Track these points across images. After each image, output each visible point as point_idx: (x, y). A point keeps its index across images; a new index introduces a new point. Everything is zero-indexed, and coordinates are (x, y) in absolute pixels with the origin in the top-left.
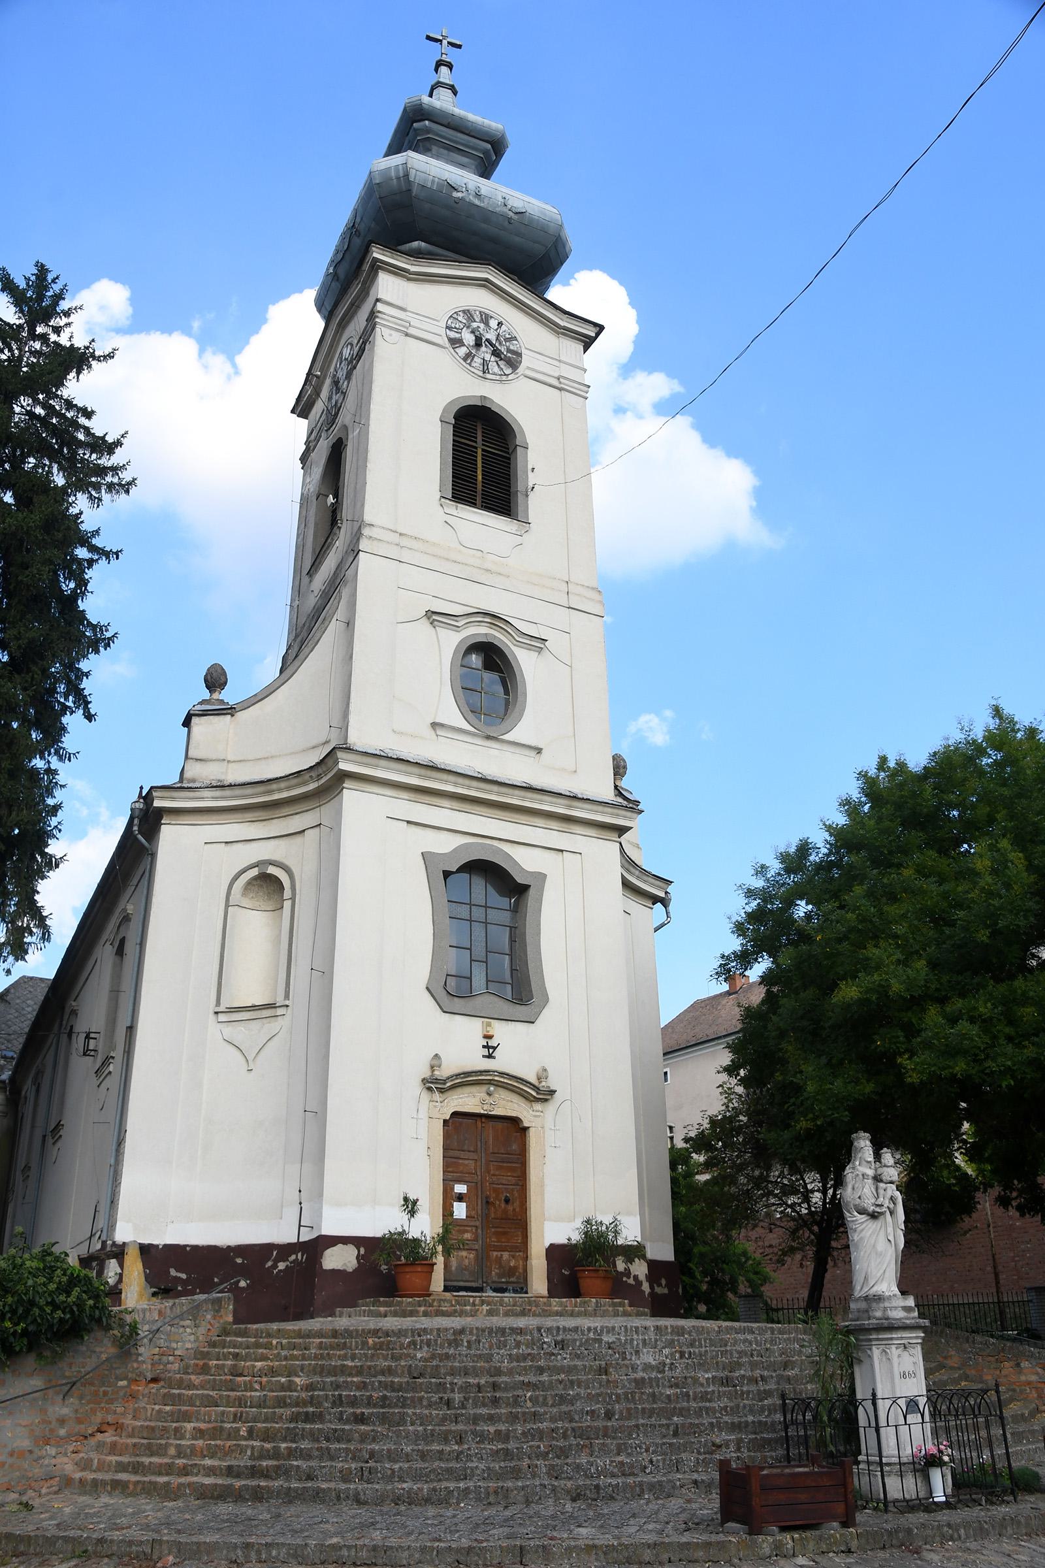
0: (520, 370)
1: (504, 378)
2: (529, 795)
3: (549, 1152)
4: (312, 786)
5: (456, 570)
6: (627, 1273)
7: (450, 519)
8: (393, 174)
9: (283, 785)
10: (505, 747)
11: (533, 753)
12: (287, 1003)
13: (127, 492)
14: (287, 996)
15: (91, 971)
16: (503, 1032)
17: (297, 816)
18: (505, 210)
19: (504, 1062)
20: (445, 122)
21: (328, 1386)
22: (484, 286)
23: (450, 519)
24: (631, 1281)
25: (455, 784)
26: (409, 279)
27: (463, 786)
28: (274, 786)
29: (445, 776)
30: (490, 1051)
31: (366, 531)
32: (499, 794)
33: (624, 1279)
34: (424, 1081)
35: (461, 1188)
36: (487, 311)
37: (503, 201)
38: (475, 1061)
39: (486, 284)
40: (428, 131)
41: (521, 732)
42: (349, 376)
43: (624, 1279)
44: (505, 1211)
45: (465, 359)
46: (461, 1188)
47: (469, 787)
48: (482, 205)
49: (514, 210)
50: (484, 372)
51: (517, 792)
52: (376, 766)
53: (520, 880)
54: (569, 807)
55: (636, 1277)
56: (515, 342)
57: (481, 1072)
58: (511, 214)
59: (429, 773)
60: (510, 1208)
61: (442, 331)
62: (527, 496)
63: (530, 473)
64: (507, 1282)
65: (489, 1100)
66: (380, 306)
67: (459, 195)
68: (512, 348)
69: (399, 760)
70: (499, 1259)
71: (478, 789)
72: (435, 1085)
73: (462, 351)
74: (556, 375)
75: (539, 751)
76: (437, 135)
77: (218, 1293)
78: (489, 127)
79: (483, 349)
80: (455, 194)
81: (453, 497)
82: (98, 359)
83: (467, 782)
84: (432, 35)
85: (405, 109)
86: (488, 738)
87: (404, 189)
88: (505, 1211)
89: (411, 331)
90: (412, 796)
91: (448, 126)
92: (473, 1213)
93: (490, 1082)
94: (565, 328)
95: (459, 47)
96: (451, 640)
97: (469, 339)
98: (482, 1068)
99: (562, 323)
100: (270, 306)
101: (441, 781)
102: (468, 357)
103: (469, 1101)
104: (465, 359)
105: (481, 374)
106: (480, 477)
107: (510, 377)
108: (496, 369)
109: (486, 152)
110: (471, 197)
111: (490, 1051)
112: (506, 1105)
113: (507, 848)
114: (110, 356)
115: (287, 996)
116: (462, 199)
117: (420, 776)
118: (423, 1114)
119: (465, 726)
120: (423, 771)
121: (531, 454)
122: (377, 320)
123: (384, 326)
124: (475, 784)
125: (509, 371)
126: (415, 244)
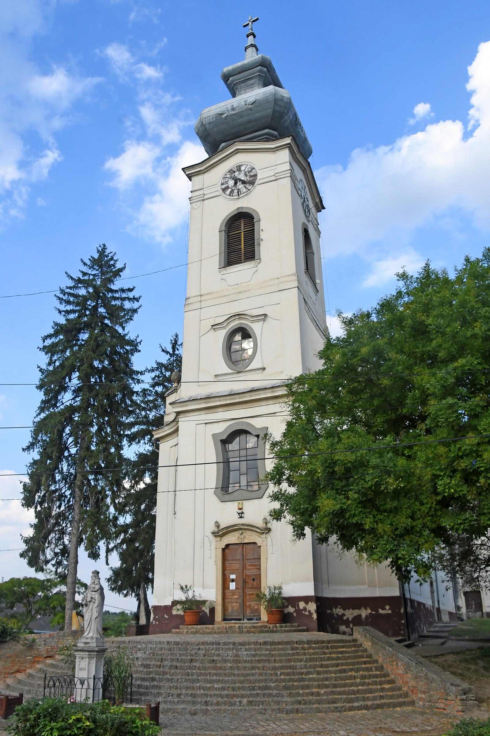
2: (253, 393)
3: (270, 556)
5: (225, 300)
6: (305, 609)
7: (223, 277)
11: (261, 371)
13: (132, 320)
18: (247, 106)
20: (237, 73)
22: (238, 152)
23: (223, 277)
24: (307, 613)
25: (220, 401)
26: (204, 173)
27: (223, 400)
29: (214, 399)
30: (241, 515)
32: (240, 398)
33: (303, 612)
34: (213, 533)
35: (233, 577)
38: (235, 520)
39: (237, 151)
40: (233, 81)
43: (303, 612)
44: (253, 585)
46: (233, 577)
47: (226, 400)
48: (236, 112)
51: (247, 394)
52: (187, 405)
54: (273, 392)
55: (309, 611)
58: (250, 106)
59: (207, 400)
60: (255, 583)
63: (261, 233)
64: (254, 616)
67: (225, 115)
68: (252, 174)
69: (193, 400)
70: (250, 606)
71: (230, 399)
73: (228, 192)
74: (273, 174)
75: (264, 369)
78: (255, 60)
79: (238, 184)
80: (223, 116)
83: (224, 398)
84: (245, 24)
86: (239, 372)
89: (206, 197)
90: (206, 411)
91: (239, 73)
92: (238, 587)
93: (241, 529)
95: (257, 19)
97: (231, 183)
99: (273, 146)
100: (469, 68)
101: (214, 401)
102: (232, 191)
103: (232, 538)
105: (237, 197)
108: (245, 190)
109: (260, 71)
111: (241, 515)
112: (250, 537)
113: (249, 421)
116: (227, 116)
117: (205, 403)
118: (213, 547)
120: (205, 401)
124: (228, 398)
126: (221, 147)
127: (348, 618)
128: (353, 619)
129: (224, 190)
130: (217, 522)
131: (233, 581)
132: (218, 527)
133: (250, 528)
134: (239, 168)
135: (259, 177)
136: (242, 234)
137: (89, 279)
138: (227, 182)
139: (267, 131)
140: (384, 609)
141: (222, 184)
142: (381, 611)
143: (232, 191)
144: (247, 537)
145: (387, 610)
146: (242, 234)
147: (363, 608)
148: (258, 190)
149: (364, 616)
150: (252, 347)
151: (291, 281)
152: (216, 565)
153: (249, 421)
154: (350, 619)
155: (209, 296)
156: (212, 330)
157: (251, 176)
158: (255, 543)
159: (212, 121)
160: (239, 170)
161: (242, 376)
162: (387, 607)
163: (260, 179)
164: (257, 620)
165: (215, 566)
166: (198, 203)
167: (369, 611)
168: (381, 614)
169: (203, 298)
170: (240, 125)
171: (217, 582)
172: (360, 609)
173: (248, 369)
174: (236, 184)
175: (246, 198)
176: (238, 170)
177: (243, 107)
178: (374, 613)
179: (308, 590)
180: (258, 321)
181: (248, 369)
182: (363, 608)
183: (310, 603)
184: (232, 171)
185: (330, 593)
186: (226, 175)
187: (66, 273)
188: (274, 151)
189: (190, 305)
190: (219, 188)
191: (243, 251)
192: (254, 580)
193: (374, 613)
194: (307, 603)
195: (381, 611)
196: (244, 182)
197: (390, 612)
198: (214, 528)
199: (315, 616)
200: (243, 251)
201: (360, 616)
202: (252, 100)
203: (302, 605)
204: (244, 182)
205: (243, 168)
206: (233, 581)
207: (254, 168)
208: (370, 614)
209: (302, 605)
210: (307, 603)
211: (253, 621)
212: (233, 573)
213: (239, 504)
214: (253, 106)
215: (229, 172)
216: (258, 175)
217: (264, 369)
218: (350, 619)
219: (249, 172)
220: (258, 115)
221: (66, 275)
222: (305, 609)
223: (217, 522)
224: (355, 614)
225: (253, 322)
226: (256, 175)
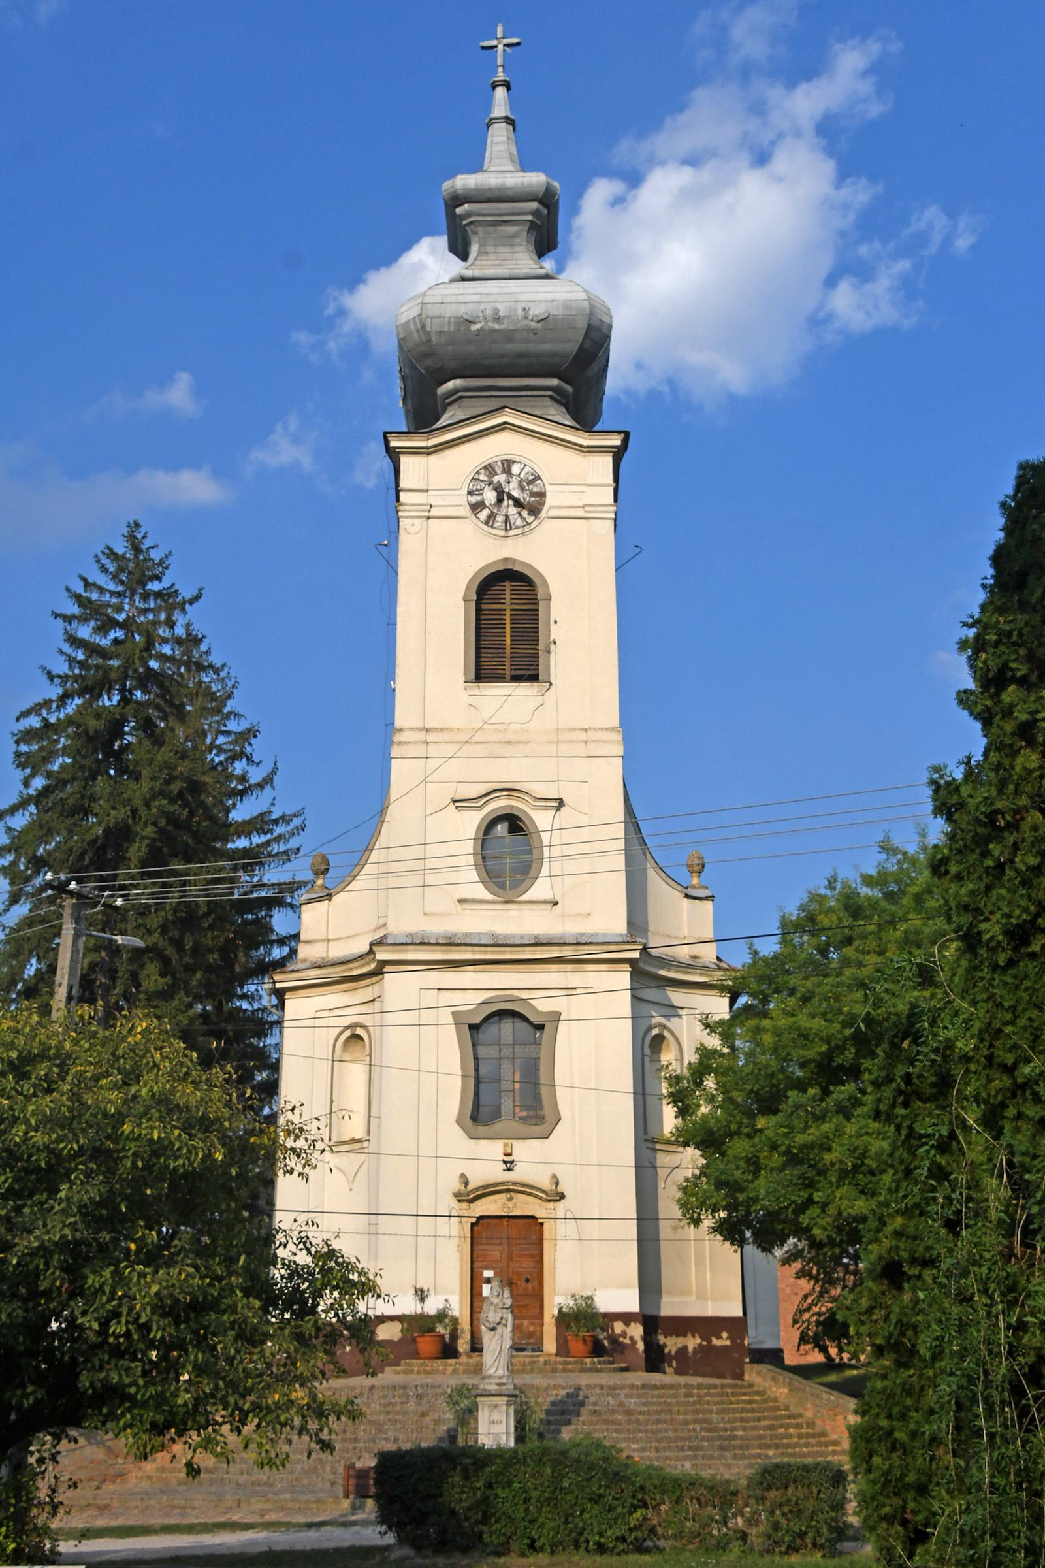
0: (543, 514)
6: (624, 1334)
8: (413, 327)
9: (356, 964)
10: (523, 906)
11: (549, 906)
14: (369, 1134)
15: (644, 1107)
16: (523, 1150)
18: (526, 322)
19: (521, 1173)
24: (627, 1341)
26: (429, 454)
28: (351, 965)
29: (463, 948)
30: (509, 1166)
35: (488, 1273)
38: (496, 1173)
39: (503, 427)
41: (540, 889)
44: (526, 1289)
46: (488, 1273)
47: (486, 952)
55: (631, 1338)
56: (539, 482)
57: (502, 1183)
58: (534, 325)
60: (530, 1286)
62: (549, 652)
63: (553, 627)
65: (510, 1204)
67: (478, 326)
68: (535, 490)
72: (468, 1195)
73: (484, 514)
75: (556, 903)
76: (480, 215)
78: (530, 185)
79: (505, 503)
82: (191, 602)
86: (507, 902)
87: (424, 339)
88: (526, 1289)
89: (434, 512)
91: (489, 201)
93: (508, 1191)
96: (471, 821)
97: (490, 496)
98: (500, 1180)
102: (491, 517)
103: (490, 1206)
104: (486, 523)
105: (502, 533)
107: (533, 525)
108: (519, 522)
110: (490, 324)
111: (509, 1166)
112: (525, 1206)
114: (197, 598)
115: (369, 1134)
116: (482, 329)
119: (490, 897)
125: (530, 519)
127: (670, 1352)
128: (677, 1352)
129: (476, 507)
130: (463, 1175)
131: (488, 1281)
132: (466, 1184)
133: (527, 1189)
134: (507, 466)
135: (549, 501)
136: (508, 613)
137: (148, 622)
138: (480, 492)
139: (555, 382)
140: (719, 1337)
141: (470, 493)
142: (715, 1341)
144: (519, 1205)
145: (723, 1341)
146: (508, 613)
147: (689, 1336)
149: (691, 1349)
151: (610, 742)
152: (461, 1252)
154: (673, 1353)
155: (445, 736)
156: (452, 806)
157: (532, 494)
158: (533, 1217)
159: (446, 329)
160: (507, 471)
161: (513, 910)
162: (725, 1335)
163: (551, 507)
164: (533, 1350)
165: (458, 1255)
166: (417, 521)
167: (698, 1340)
168: (715, 1346)
170: (503, 356)
171: (461, 1283)
172: (685, 1336)
173: (520, 899)
174: (500, 501)
175: (521, 540)
176: (504, 471)
177: (519, 322)
178: (705, 1343)
179: (629, 1301)
180: (546, 808)
181: (520, 899)
182: (689, 1336)
183: (633, 1324)
184: (489, 469)
185: (670, 1307)
186: (478, 473)
187: (68, 589)
189: (405, 747)
190: (463, 499)
191: (508, 651)
192: (527, 1281)
193: (705, 1343)
194: (627, 1324)
195: (715, 1341)
196: (518, 503)
197: (728, 1343)
198: (457, 1186)
199: (641, 1346)
200: (508, 651)
201: (685, 1348)
203: (618, 1327)
204: (518, 503)
205: (515, 469)
206: (488, 1281)
207: (538, 478)
208: (700, 1345)
209: (618, 1327)
210: (627, 1324)
211: (526, 1353)
212: (488, 1268)
213: (506, 1145)
214: (540, 325)
215: (485, 468)
216: (548, 494)
217: (556, 903)
218: (673, 1353)
219: (530, 482)
220: (547, 347)
221: (66, 594)
222: (624, 1334)
223: (463, 1175)
224: (680, 1345)
225: (536, 808)
226: (542, 495)
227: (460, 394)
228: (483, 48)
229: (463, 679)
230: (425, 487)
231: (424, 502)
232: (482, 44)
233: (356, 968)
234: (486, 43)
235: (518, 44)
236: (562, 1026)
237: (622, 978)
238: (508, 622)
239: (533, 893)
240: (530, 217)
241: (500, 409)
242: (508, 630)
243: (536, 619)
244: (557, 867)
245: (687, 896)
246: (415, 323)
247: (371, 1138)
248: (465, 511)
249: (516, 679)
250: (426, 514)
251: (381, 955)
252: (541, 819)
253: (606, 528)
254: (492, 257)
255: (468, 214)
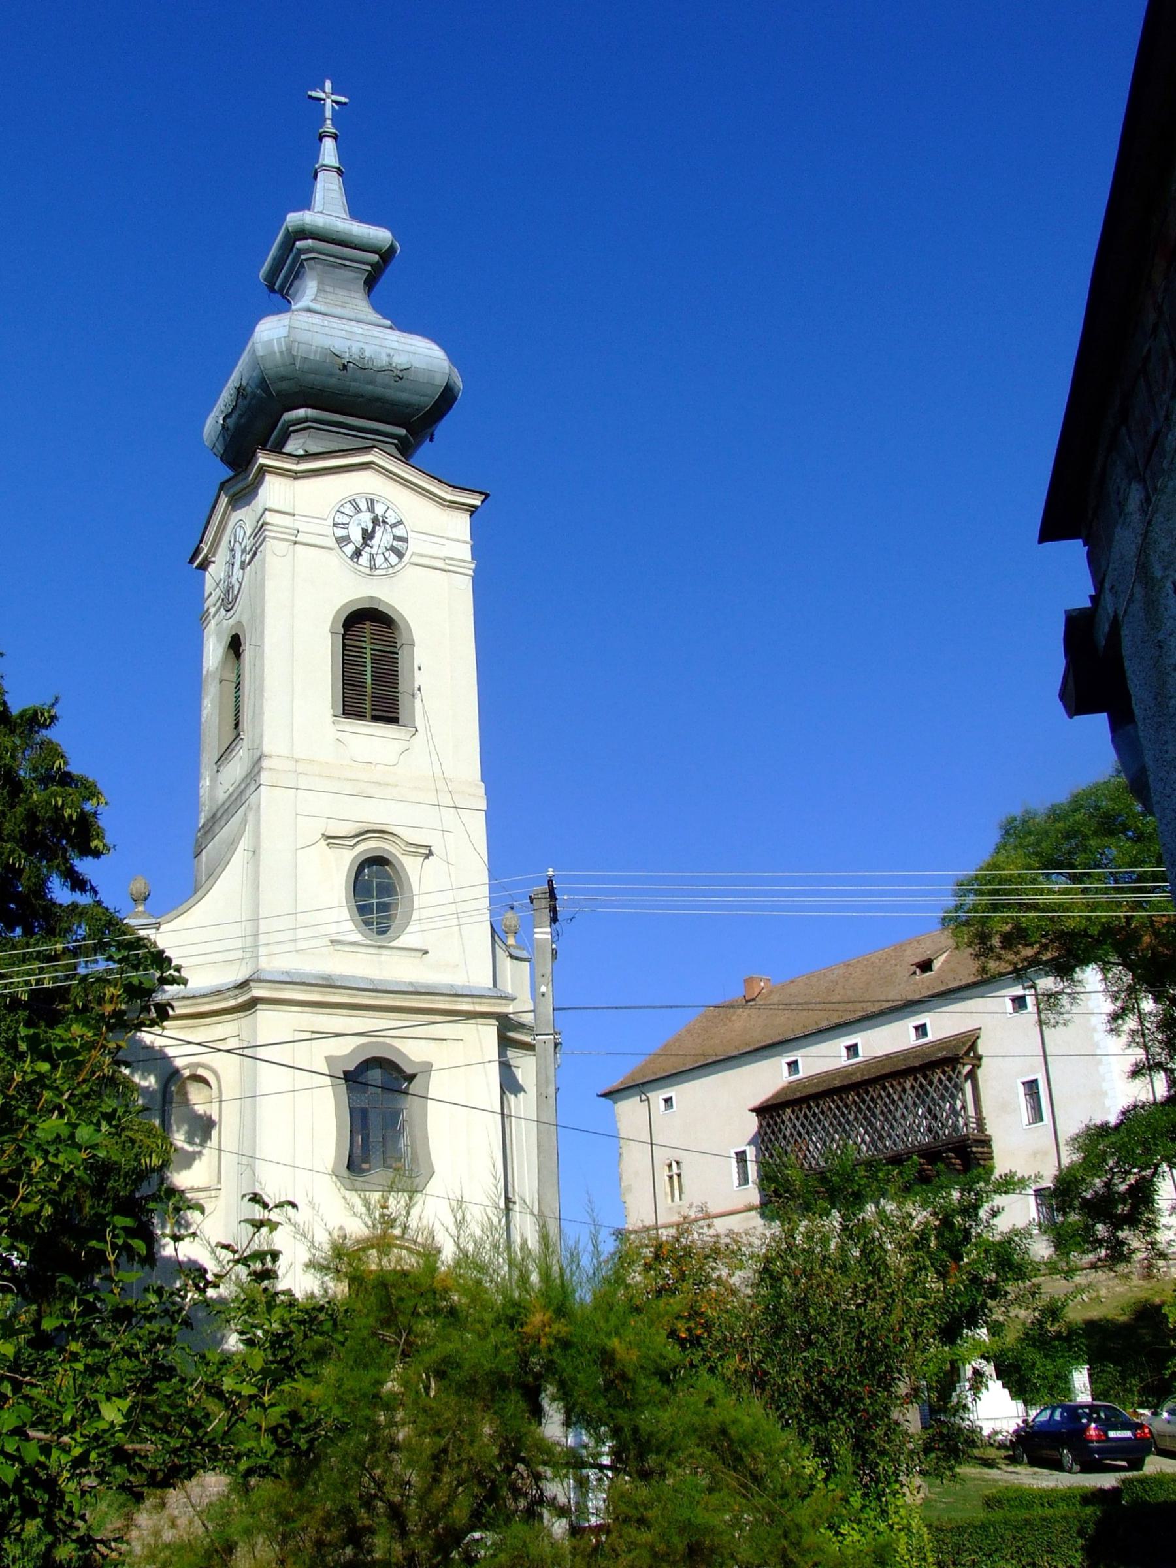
0: (406, 559)
1: (391, 571)
4: (232, 1003)
12: (219, 1187)
14: (219, 1182)
17: (220, 1025)
21: (939, 1093)
26: (295, 478)
31: (265, 763)
36: (372, 497)
37: (387, 359)
41: (408, 939)
42: (249, 563)
45: (352, 558)
49: (398, 367)
50: (371, 568)
53: (409, 1070)
61: (328, 530)
66: (269, 517)
75: (426, 952)
77: (223, 757)
81: (344, 714)
85: (210, 1139)
89: (300, 538)
94: (450, 502)
96: (345, 860)
99: (448, 497)
102: (358, 553)
104: (352, 558)
105: (367, 571)
106: (369, 681)
107: (397, 569)
121: (417, 650)
122: (267, 533)
123: (274, 538)
141: (335, 525)
143: (358, 553)
148: (410, 576)
150: (414, 912)
153: (397, 1043)
156: (323, 843)
163: (413, 554)
169: (301, 767)
173: (392, 944)
180: (416, 854)
181: (392, 944)
188: (444, 506)
202: (400, 361)
217: (426, 952)
221: (683, 1196)
227: (309, 424)
228: (310, 97)
229: (331, 712)
230: (291, 511)
231: (291, 525)
232: (310, 93)
233: (203, 1004)
234: (313, 94)
235: (345, 104)
236: (434, 1076)
237: (489, 1033)
238: (369, 661)
239: (404, 940)
240: (369, 268)
241: (367, 449)
242: (369, 669)
243: (395, 662)
244: (425, 913)
245: (511, 956)
246: (279, 344)
247: (222, 1186)
248: (332, 543)
249: (375, 718)
250: (293, 538)
251: (258, 992)
252: (411, 865)
253: (464, 586)
254: (330, 296)
255: (309, 250)
